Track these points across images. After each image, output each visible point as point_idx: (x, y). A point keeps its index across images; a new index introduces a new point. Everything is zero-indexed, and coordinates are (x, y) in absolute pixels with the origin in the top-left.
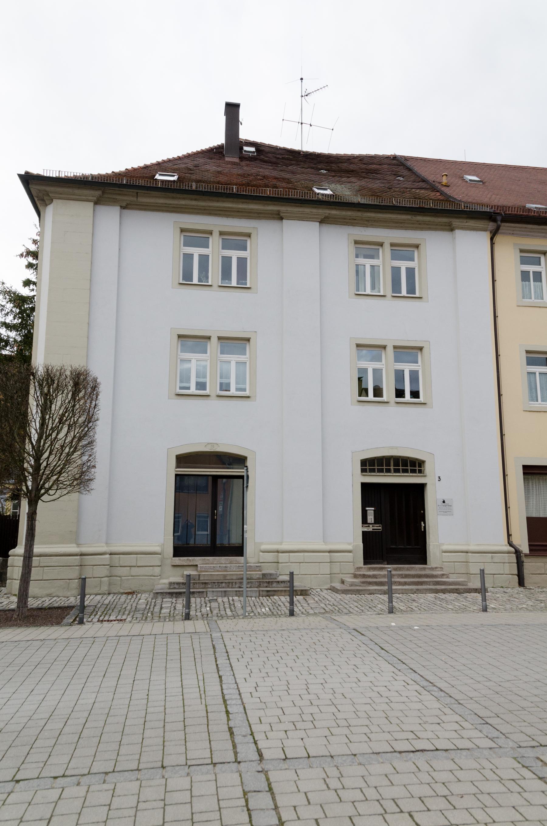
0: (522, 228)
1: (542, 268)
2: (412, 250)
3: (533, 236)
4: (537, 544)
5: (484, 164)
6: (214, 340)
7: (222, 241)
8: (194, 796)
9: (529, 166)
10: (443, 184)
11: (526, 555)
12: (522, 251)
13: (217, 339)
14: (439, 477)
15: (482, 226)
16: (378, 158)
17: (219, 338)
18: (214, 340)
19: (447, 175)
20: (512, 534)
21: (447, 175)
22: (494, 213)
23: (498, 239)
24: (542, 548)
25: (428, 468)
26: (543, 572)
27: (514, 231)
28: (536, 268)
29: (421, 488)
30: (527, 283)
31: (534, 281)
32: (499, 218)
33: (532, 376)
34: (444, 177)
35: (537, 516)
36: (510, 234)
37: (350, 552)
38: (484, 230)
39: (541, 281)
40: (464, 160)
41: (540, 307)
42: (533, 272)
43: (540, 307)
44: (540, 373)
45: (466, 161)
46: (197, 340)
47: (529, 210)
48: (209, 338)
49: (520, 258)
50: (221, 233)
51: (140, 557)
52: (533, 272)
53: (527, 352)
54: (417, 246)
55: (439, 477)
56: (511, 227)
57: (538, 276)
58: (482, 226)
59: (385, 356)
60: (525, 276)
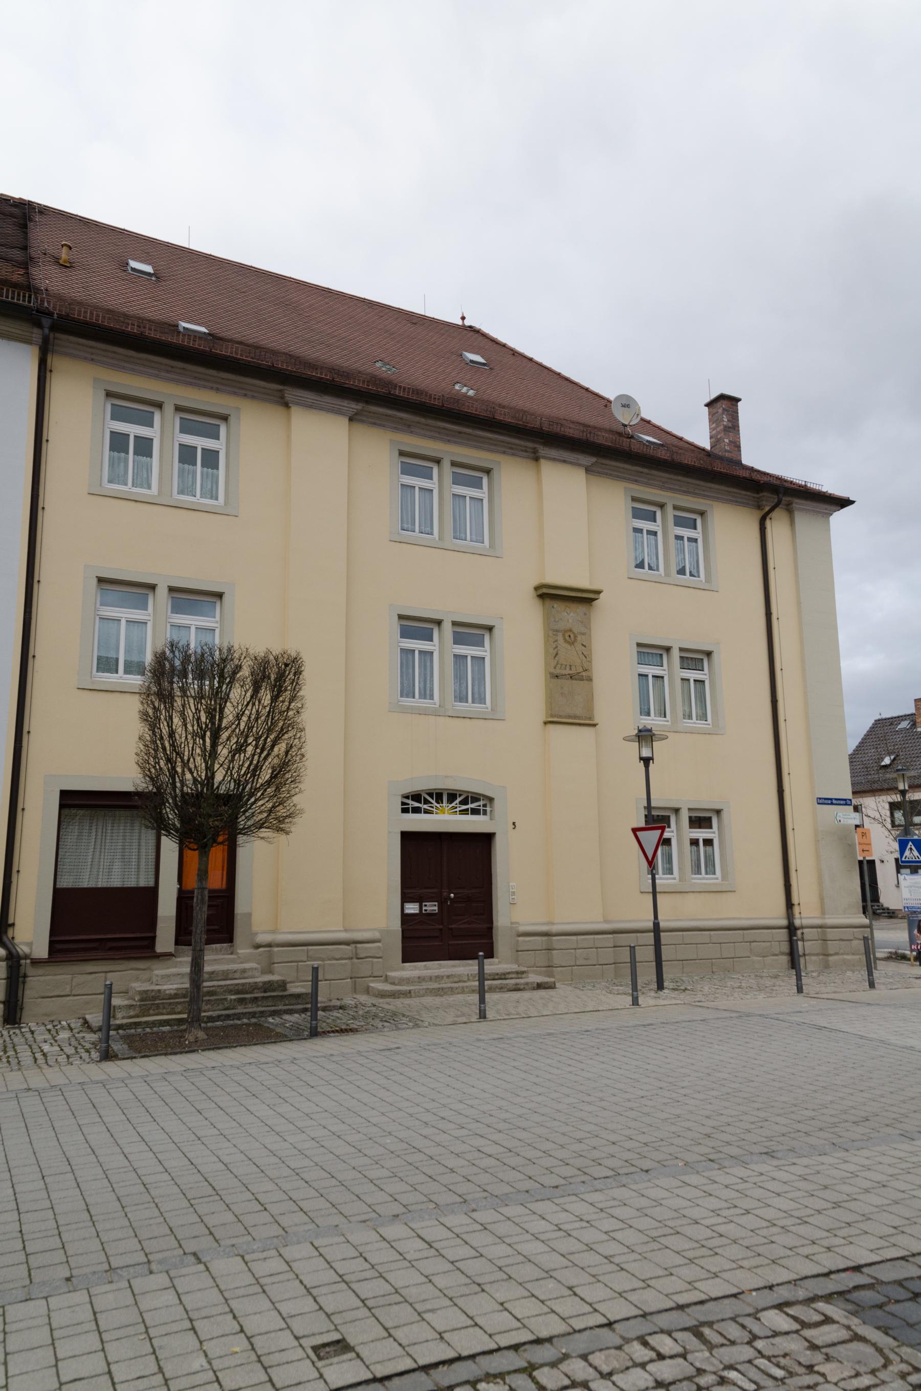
0: (106, 351)
1: (698, 533)
2: (217, 423)
3: (133, 370)
4: (67, 938)
5: (363, 301)
6: (162, 592)
7: (112, 408)
8: (52, 1366)
9: (292, 277)
10: (61, 262)
11: (36, 962)
12: (402, 454)
13: (166, 591)
14: (514, 823)
15: (20, 332)
16: (179, 252)
17: (172, 589)
18: (162, 592)
19: (70, 248)
20: (17, 923)
21: (70, 248)
22: (37, 311)
23: (56, 362)
24: (132, 943)
25: (400, 810)
26: (67, 992)
27: (92, 354)
28: (210, 444)
29: (486, 840)
30: (123, 455)
31: (203, 466)
32: (46, 322)
33: (686, 683)
34: (65, 249)
35: (90, 886)
36: (85, 358)
37: (378, 941)
38: (28, 341)
39: (150, 455)
40: (423, 313)
41: (136, 501)
42: (135, 436)
43: (136, 501)
44: (653, 676)
45: (191, 248)
46: (134, 590)
47: (641, 442)
48: (152, 587)
49: (633, 511)
50: (454, 464)
51: (558, 940)
52: (135, 436)
53: (401, 617)
54: (225, 418)
55: (514, 823)
56: (83, 345)
57: (211, 458)
58: (20, 332)
59: (439, 639)
60: (118, 442)
